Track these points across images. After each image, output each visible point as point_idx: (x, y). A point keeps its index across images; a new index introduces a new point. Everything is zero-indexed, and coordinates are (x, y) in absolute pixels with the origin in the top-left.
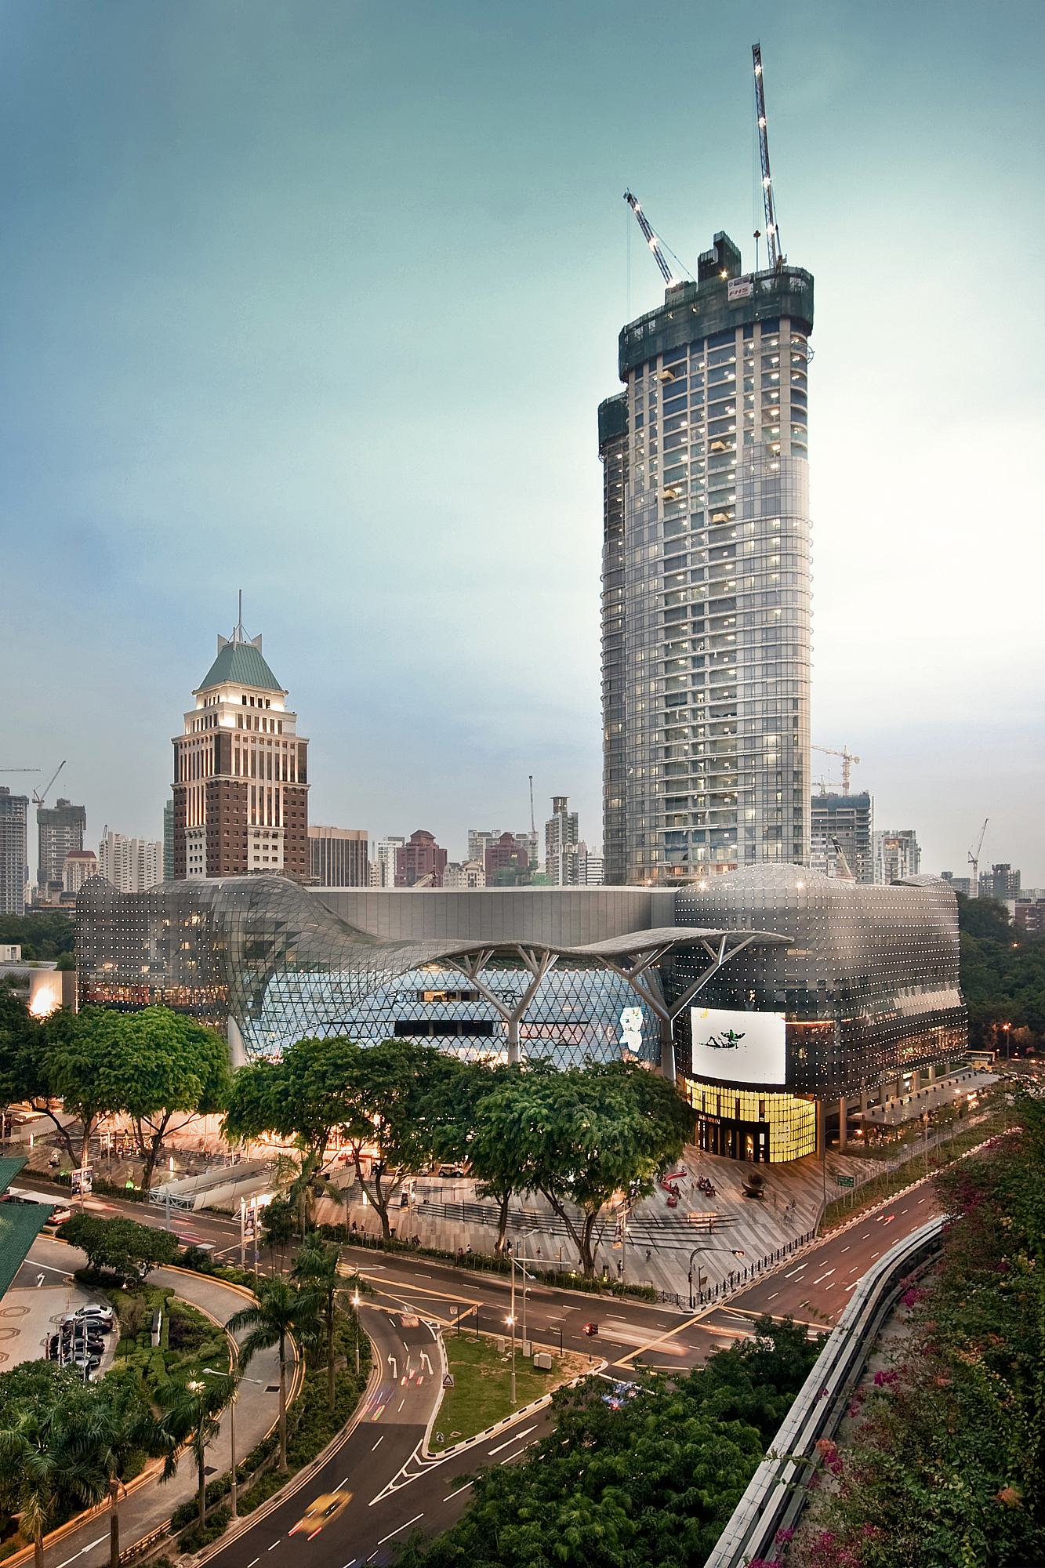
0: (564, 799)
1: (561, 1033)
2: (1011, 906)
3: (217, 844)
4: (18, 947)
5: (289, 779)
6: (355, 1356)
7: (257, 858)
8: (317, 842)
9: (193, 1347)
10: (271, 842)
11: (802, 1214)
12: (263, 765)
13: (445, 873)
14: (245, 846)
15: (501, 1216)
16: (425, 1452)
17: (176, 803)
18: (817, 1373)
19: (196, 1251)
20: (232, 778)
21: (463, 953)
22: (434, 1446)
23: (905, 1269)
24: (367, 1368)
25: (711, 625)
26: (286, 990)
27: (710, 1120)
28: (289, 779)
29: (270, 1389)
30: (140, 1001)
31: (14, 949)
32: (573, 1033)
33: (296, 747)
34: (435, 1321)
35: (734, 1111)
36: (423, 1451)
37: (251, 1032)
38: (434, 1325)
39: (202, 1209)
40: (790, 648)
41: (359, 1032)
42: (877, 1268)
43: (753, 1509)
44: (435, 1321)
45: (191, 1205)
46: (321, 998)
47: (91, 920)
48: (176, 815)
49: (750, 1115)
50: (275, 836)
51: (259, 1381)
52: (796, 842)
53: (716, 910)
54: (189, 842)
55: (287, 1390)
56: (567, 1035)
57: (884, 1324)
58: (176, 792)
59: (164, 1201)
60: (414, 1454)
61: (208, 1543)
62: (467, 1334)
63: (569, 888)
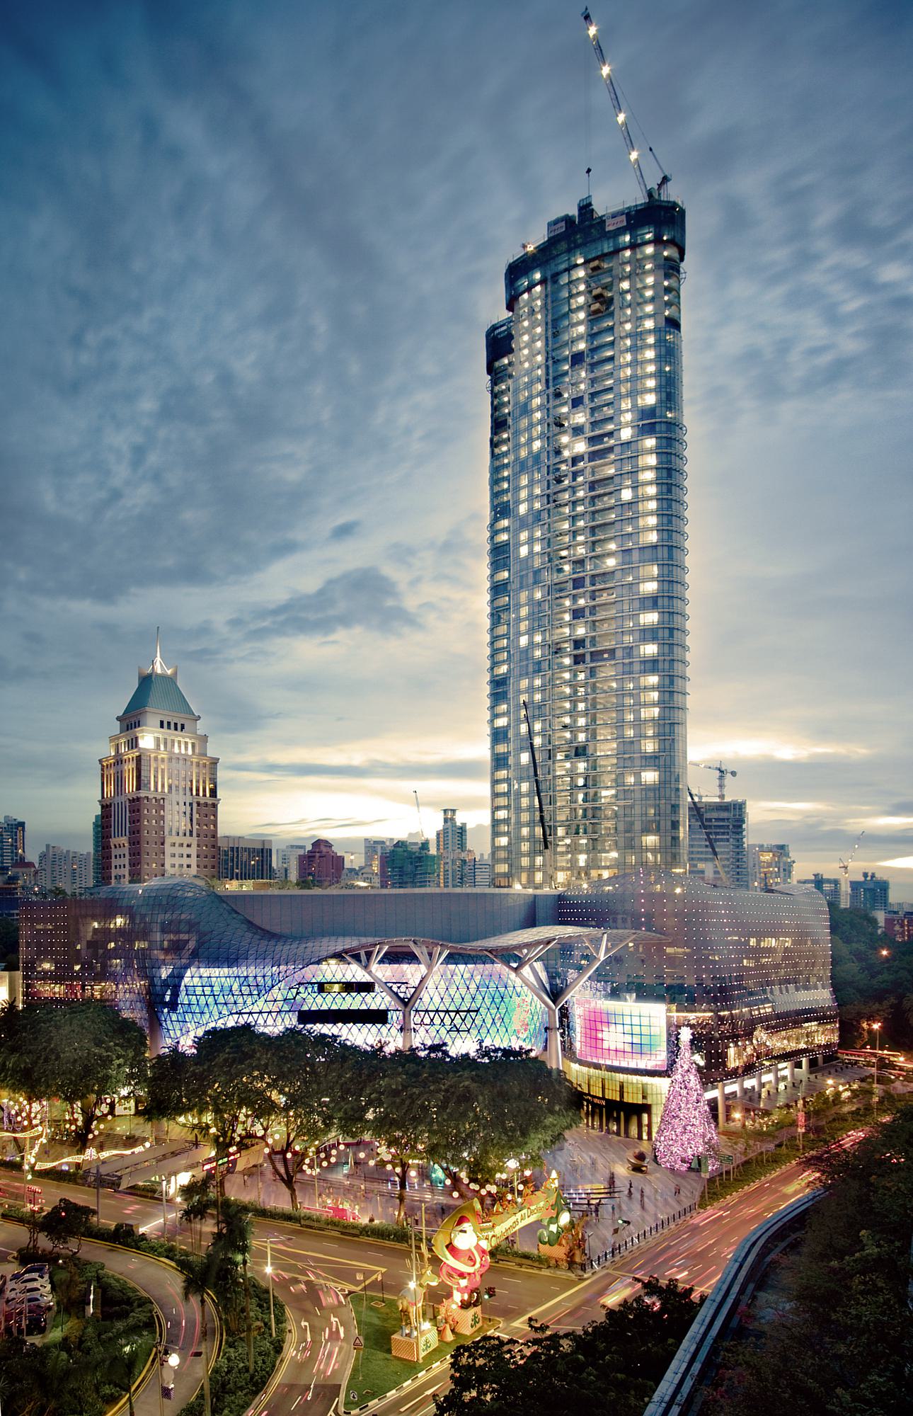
0: (454, 811)
1: (452, 1020)
2: (881, 916)
5: (201, 794)
6: (270, 1320)
9: (123, 1315)
10: (185, 851)
13: (343, 877)
17: (103, 818)
18: (696, 1329)
26: (200, 984)
27: (596, 1101)
28: (201, 794)
30: (73, 997)
32: (463, 1020)
34: (343, 1287)
35: (618, 1093)
37: (169, 1022)
38: (343, 1290)
41: (265, 1022)
44: (343, 1287)
46: (231, 991)
47: (32, 924)
49: (632, 1098)
53: (597, 911)
56: (458, 1021)
58: (103, 807)
63: (458, 890)
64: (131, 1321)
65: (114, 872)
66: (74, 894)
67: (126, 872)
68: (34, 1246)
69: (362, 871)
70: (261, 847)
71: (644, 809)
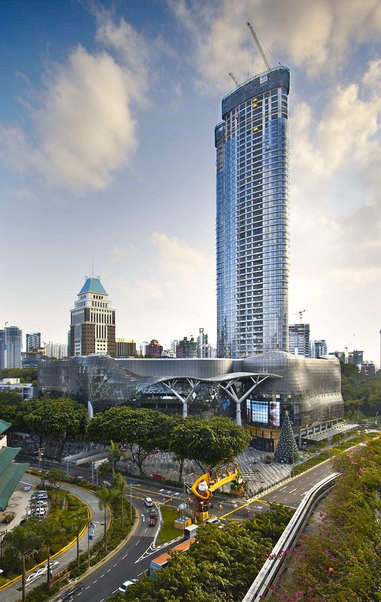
2: (360, 366)
3: (85, 341)
4: (19, 379)
7: (98, 349)
8: (119, 343)
10: (103, 344)
11: (286, 470)
12: (100, 318)
14: (94, 345)
15: (181, 467)
16: (154, 546)
19: (77, 479)
20: (90, 323)
21: (168, 380)
22: (157, 544)
23: (322, 491)
24: (134, 518)
25: (254, 299)
29: (101, 524)
31: (17, 380)
33: (112, 312)
36: (153, 546)
39: (79, 465)
40: (281, 233)
42: (311, 490)
43: (266, 571)
45: (75, 463)
48: (71, 335)
50: (104, 342)
51: (98, 522)
52: (283, 343)
54: (76, 344)
55: (107, 525)
57: (314, 509)
59: (66, 462)
60: (150, 547)
61: (80, 575)
62: (169, 507)
63: (205, 359)
64: (79, 512)
65: (75, 352)
66: (59, 359)
67: (80, 351)
68: (43, 484)
69: (170, 351)
70: (132, 342)
71: (273, 328)
